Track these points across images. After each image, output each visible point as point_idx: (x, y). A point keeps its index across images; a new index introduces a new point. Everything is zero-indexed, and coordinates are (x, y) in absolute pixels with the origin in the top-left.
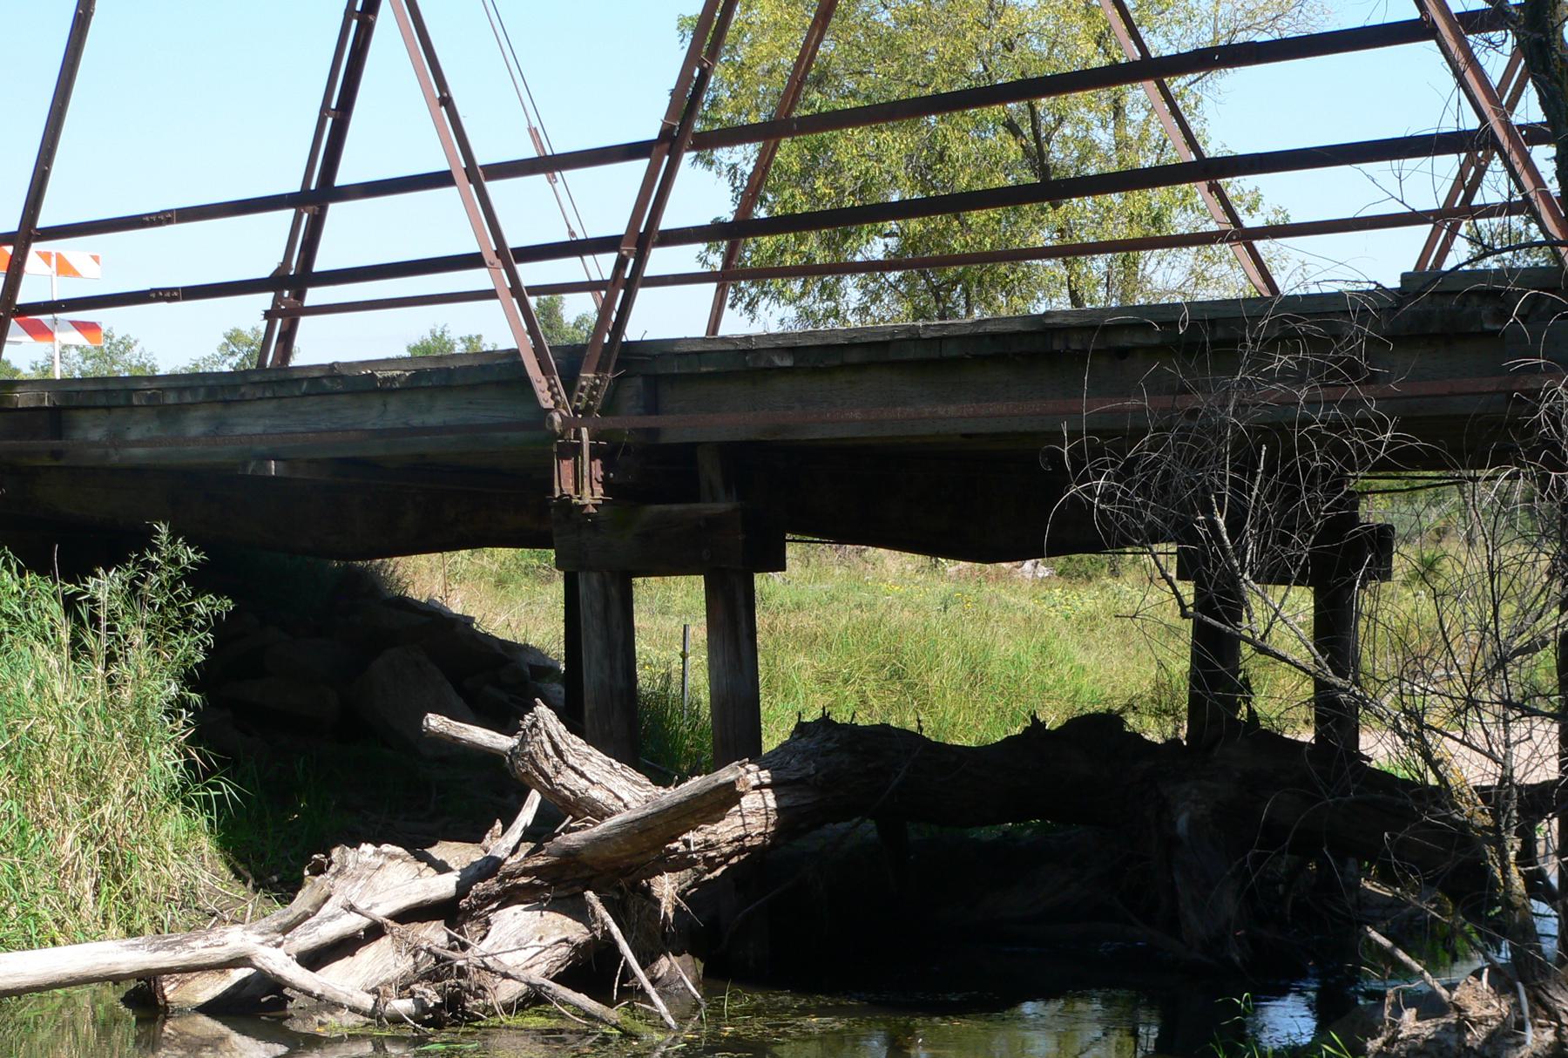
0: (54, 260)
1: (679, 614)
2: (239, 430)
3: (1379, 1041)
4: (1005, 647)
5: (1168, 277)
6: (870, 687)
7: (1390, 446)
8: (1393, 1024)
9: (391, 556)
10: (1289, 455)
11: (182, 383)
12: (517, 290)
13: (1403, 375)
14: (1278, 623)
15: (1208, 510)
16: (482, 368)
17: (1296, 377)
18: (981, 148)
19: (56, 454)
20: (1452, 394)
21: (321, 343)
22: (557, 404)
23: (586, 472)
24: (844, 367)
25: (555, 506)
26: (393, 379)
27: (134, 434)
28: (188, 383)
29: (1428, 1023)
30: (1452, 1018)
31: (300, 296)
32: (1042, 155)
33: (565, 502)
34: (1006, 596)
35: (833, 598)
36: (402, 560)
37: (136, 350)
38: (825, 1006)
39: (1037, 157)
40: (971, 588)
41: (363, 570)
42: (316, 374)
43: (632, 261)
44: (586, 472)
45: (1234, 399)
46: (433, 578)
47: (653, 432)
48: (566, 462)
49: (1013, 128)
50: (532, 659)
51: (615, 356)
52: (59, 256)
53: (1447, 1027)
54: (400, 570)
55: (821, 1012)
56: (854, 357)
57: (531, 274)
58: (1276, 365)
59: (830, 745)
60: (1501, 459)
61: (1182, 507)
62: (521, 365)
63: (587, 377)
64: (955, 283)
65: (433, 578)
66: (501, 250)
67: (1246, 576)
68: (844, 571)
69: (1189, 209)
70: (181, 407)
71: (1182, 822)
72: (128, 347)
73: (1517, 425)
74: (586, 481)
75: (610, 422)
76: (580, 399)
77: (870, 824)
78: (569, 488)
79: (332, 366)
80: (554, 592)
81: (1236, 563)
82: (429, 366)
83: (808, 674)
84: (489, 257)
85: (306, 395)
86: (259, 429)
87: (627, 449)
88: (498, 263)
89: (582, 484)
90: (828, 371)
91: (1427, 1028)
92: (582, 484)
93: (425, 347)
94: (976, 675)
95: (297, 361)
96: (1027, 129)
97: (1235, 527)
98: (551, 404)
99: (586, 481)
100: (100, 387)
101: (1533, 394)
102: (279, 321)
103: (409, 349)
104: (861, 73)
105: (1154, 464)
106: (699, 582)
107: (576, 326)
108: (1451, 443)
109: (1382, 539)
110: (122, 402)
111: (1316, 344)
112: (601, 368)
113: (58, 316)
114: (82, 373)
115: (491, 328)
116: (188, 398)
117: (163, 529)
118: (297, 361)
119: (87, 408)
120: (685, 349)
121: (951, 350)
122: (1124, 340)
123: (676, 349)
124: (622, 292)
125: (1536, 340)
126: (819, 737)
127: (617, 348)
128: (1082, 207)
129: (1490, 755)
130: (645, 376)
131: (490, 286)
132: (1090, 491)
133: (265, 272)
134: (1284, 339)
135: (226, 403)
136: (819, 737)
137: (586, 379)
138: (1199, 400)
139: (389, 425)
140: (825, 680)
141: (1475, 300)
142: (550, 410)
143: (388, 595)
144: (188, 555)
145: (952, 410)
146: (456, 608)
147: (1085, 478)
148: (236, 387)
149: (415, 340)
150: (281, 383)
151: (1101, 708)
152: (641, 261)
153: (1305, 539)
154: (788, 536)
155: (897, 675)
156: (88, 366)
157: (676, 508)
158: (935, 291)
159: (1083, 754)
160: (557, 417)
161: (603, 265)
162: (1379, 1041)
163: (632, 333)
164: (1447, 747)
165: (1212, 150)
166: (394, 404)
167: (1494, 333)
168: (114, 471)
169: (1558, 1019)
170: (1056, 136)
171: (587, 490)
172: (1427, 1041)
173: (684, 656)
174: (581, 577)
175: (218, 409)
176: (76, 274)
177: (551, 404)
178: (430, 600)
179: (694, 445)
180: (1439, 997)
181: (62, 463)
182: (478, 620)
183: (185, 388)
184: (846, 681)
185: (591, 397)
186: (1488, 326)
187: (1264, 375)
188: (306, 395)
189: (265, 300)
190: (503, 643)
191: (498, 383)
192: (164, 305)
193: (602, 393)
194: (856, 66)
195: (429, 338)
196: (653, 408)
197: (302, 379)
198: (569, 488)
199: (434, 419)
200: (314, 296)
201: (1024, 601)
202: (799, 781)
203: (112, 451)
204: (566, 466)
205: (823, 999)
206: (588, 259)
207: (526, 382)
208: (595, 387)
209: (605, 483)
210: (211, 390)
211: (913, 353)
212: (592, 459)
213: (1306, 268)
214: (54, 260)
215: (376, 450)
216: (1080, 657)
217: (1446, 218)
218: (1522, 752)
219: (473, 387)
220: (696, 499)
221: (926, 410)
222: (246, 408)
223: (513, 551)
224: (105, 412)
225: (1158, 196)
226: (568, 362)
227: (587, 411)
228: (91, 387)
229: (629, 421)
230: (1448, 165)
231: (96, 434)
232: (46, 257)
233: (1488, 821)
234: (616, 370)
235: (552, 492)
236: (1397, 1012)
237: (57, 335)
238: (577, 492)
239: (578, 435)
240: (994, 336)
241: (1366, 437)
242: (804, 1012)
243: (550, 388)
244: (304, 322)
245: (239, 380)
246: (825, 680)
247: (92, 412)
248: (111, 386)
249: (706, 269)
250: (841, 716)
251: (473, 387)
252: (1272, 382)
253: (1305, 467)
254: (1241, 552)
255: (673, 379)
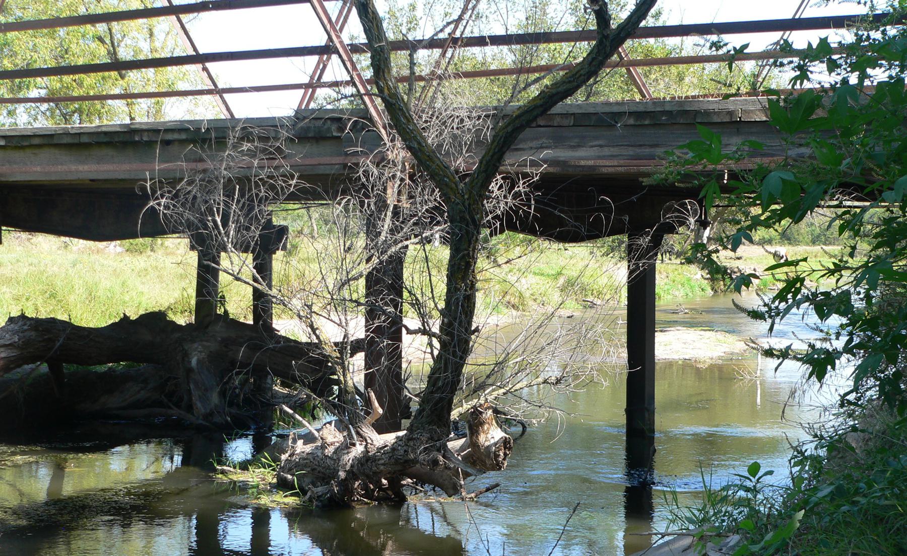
3: (287, 455)
4: (105, 284)
5: (176, 111)
6: (39, 302)
7: (295, 186)
8: (293, 447)
10: (250, 190)
13: (299, 155)
14: (245, 267)
15: (213, 215)
17: (252, 154)
18: (84, 46)
20: (320, 164)
24: (31, 146)
29: (308, 446)
30: (319, 444)
32: (115, 53)
34: (102, 260)
35: (18, 261)
38: (24, 451)
39: (113, 53)
40: (85, 257)
45: (227, 163)
49: (101, 40)
53: (317, 448)
55: (23, 453)
56: (36, 141)
58: (245, 148)
59: (25, 327)
60: (344, 193)
61: (201, 214)
64: (74, 112)
67: (230, 246)
68: (21, 248)
69: (190, 76)
71: (194, 361)
73: (350, 179)
77: (45, 365)
81: (226, 239)
83: (7, 296)
90: (22, 148)
91: (308, 448)
94: (91, 296)
96: (108, 41)
97: (225, 224)
101: (357, 165)
104: (24, 8)
105: (189, 192)
108: (320, 187)
109: (283, 230)
111: (264, 139)
121: (85, 139)
122: (169, 137)
125: (357, 139)
126: (20, 324)
128: (133, 75)
129: (340, 325)
132: (159, 204)
134: (246, 136)
136: (20, 324)
138: (209, 165)
140: (17, 299)
141: (329, 122)
145: (86, 167)
147: (157, 198)
151: (156, 309)
153: (257, 228)
154: (4, 228)
155: (53, 296)
158: (64, 115)
159: (145, 333)
162: (287, 455)
164: (319, 322)
165: (202, 51)
167: (339, 137)
169: (366, 440)
170: (122, 44)
172: (308, 454)
180: (313, 434)
184: (27, 299)
186: (335, 134)
187: (239, 152)
194: (21, 5)
201: (111, 263)
202: (10, 345)
205: (23, 448)
211: (66, 140)
213: (247, 108)
216: (140, 288)
217: (313, 85)
218: (352, 324)
221: (73, 168)
225: (172, 71)
230: (312, 60)
233: (338, 355)
236: (295, 441)
240: (106, 133)
241: (285, 182)
242: (14, 454)
246: (17, 299)
250: (30, 314)
252: (243, 155)
253: (257, 195)
254: (227, 234)
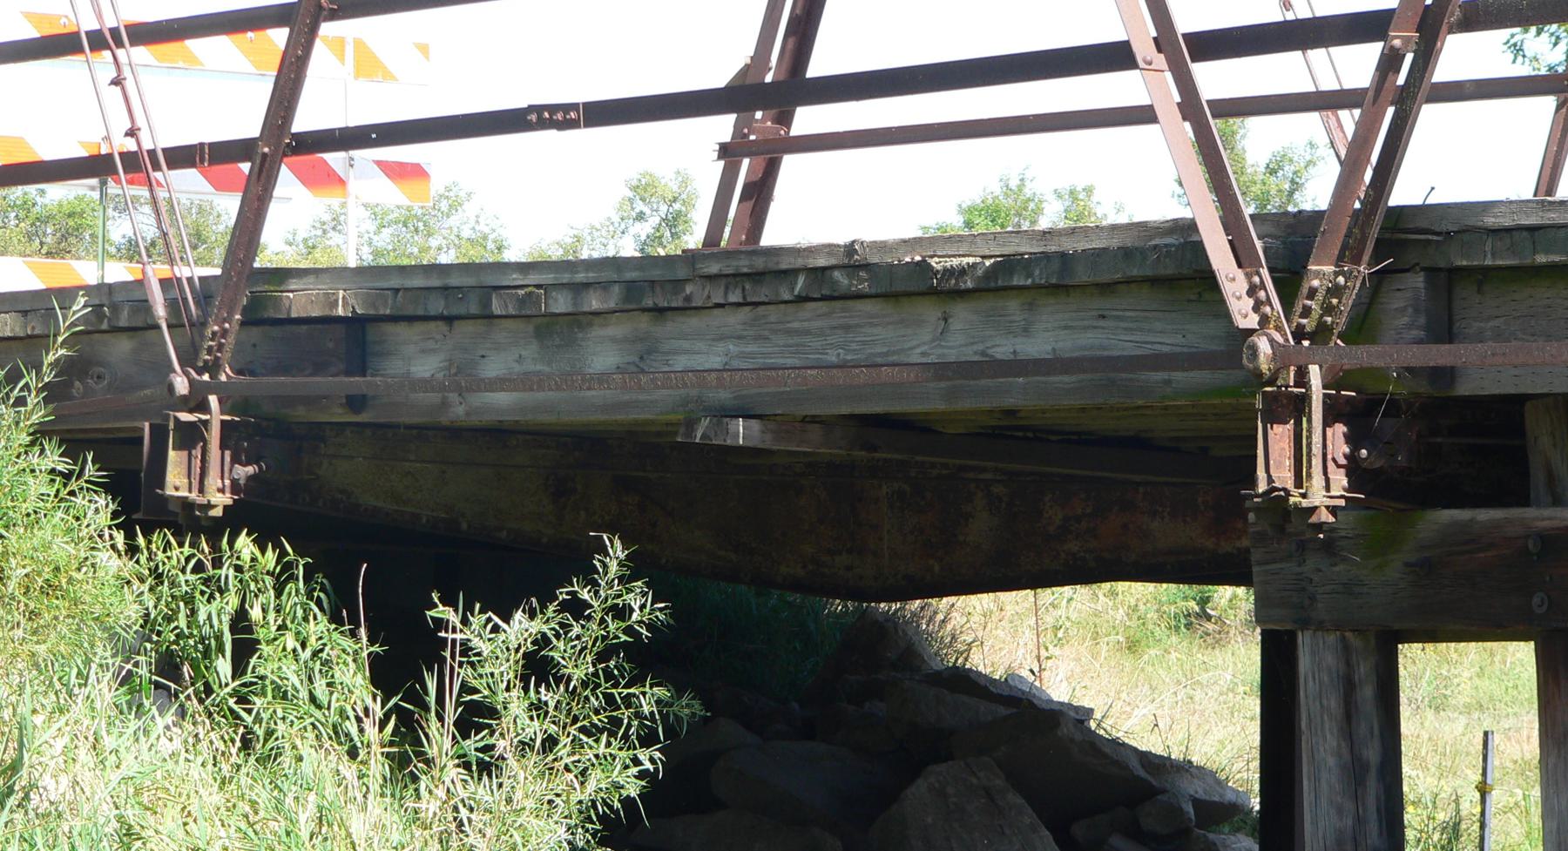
0: (349, 51)
1: (1468, 709)
2: (681, 363)
9: (941, 594)
11: (581, 277)
12: (1190, 105)
16: (1127, 253)
19: (356, 402)
21: (818, 206)
22: (1264, 320)
23: (1317, 449)
25: (1258, 509)
26: (962, 272)
27: (492, 368)
28: (592, 276)
31: (785, 119)
33: (1276, 503)
36: (961, 601)
37: (470, 210)
41: (891, 619)
42: (822, 262)
43: (1409, 57)
44: (1317, 449)
46: (1004, 634)
47: (1444, 375)
48: (1278, 429)
50: (1196, 788)
51: (1374, 232)
52: (359, 45)
54: (957, 620)
57: (1218, 79)
62: (1199, 249)
63: (1321, 272)
65: (1004, 634)
66: (1165, 39)
70: (579, 320)
72: (455, 206)
74: (1317, 463)
75: (1363, 356)
76: (1306, 312)
78: (1284, 476)
79: (850, 249)
80: (1241, 661)
82: (1027, 248)
84: (1144, 48)
85: (802, 299)
86: (715, 361)
87: (1394, 408)
88: (1160, 61)
89: (1306, 466)
92: (1306, 466)
93: (992, 212)
95: (771, 236)
98: (1252, 321)
99: (1317, 463)
100: (436, 282)
102: (746, 162)
103: (961, 211)
106: (1520, 657)
107: (1271, 171)
110: (474, 309)
112: (1348, 254)
113: (357, 154)
114: (376, 253)
115: (1134, 181)
116: (594, 302)
117: (617, 550)
118: (771, 236)
119: (411, 319)
120: (1507, 222)
123: (1490, 221)
124: (1391, 111)
127: (1379, 219)
130: (1431, 271)
131: (1142, 99)
133: (718, 77)
135: (659, 312)
137: (1317, 274)
139: (952, 356)
142: (1251, 332)
143: (936, 665)
144: (641, 605)
146: (1058, 690)
148: (678, 284)
149: (973, 195)
150: (757, 277)
152: (1427, 54)
154: (1262, 487)
156: (384, 239)
157: (1484, 515)
160: (1264, 346)
161: (1356, 65)
163: (1403, 194)
166: (963, 315)
168: (455, 433)
171: (1318, 481)
173: (1483, 790)
174: (1304, 641)
175: (644, 322)
176: (388, 76)
177: (1252, 321)
178: (1012, 675)
179: (1520, 400)
181: (363, 418)
182: (1097, 715)
183: (586, 286)
185: (1328, 309)
188: (802, 299)
189: (722, 126)
190: (1146, 758)
191: (1154, 282)
192: (551, 135)
193: (1348, 301)
195: (998, 192)
196: (1443, 330)
197: (794, 272)
198: (1284, 476)
199: (1037, 346)
200: (809, 119)
203: (453, 397)
204: (1280, 437)
206: (1317, 55)
207: (1207, 280)
208: (1336, 291)
209: (1353, 468)
210: (632, 290)
212: (1327, 423)
214: (349, 51)
215: (929, 401)
219: (1106, 288)
220: (1522, 499)
222: (693, 322)
223: (1151, 587)
224: (442, 326)
226: (1289, 245)
227: (1320, 334)
228: (418, 282)
229: (1399, 354)
231: (426, 366)
232: (338, 45)
234: (1377, 258)
235: (1253, 482)
237: (353, 185)
238: (1299, 483)
239: (1302, 378)
243: (1252, 291)
244: (791, 165)
245: (681, 273)
247: (420, 327)
248: (454, 281)
249: (1522, 70)
251: (1106, 288)
255: (1483, 276)
